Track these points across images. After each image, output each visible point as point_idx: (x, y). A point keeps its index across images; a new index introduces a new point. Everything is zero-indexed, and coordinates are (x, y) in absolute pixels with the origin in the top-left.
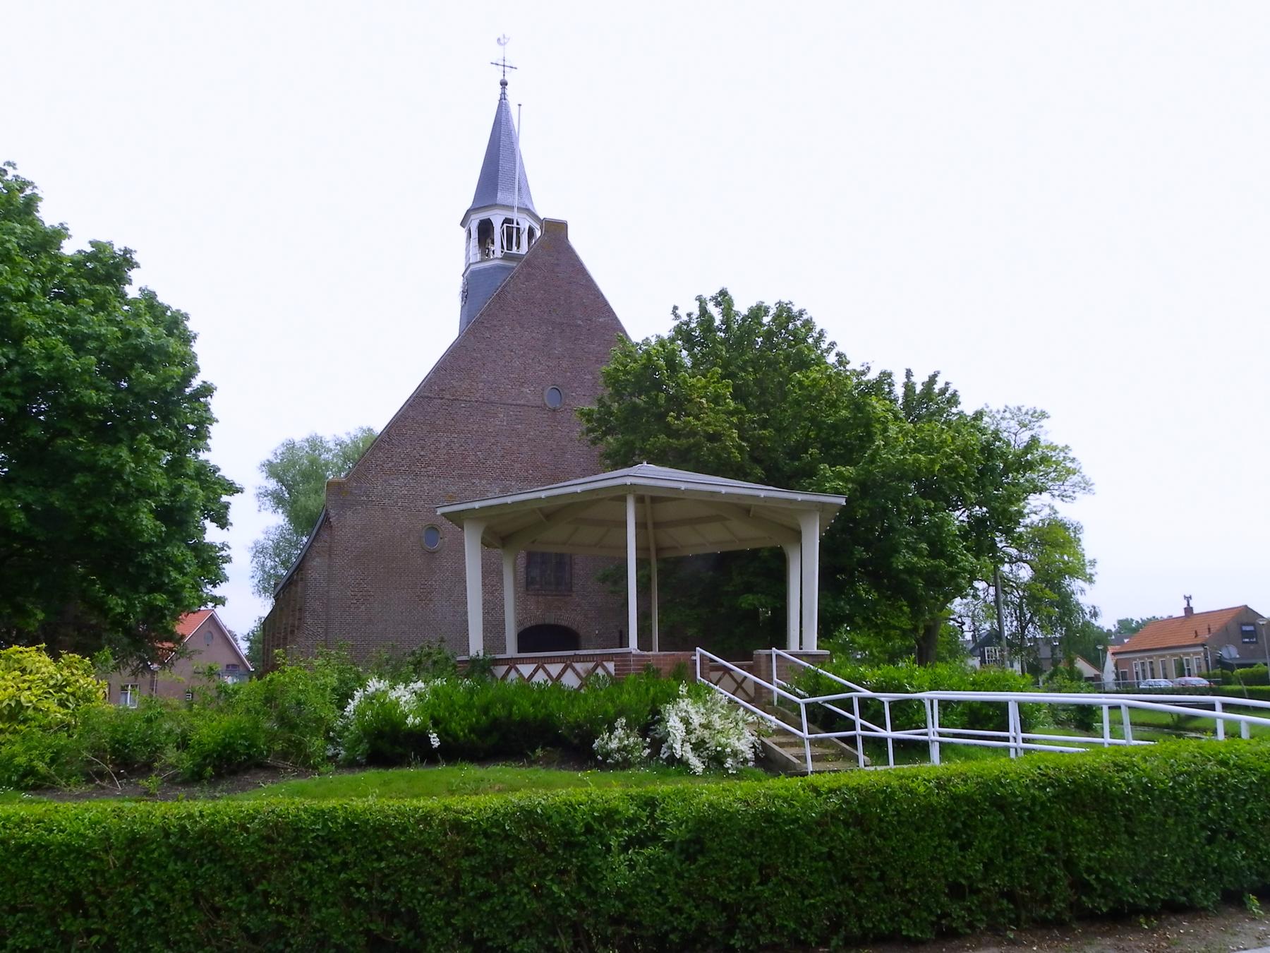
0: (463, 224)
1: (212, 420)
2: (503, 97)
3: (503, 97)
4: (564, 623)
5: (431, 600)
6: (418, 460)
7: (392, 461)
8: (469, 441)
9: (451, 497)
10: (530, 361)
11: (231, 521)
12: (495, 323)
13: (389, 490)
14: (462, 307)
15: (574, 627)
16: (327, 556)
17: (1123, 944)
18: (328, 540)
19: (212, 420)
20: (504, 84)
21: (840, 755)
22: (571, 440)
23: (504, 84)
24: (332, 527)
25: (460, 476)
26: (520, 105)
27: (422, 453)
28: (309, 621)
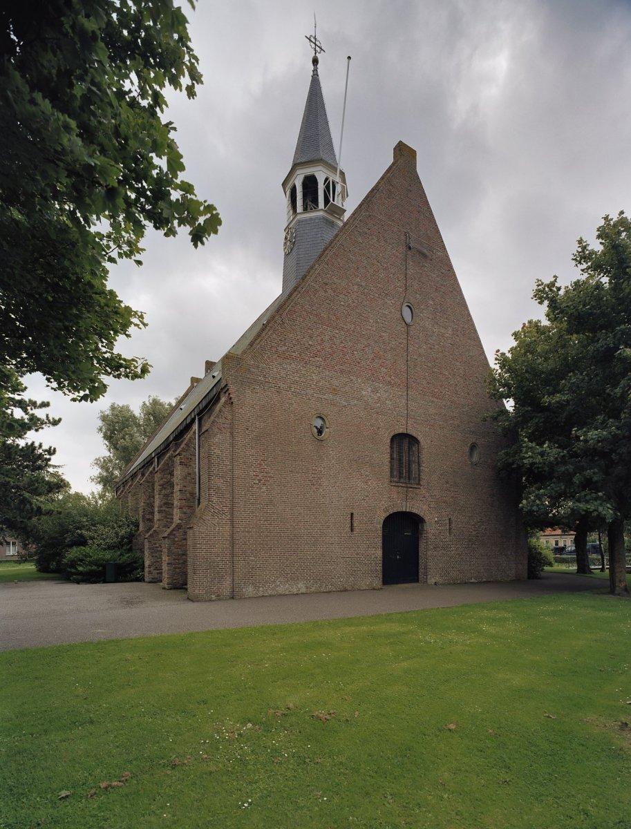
0: (284, 185)
1: (216, 232)
2: (315, 70)
3: (315, 70)
4: (415, 511)
5: (320, 485)
6: (307, 349)
7: (285, 345)
8: (348, 339)
9: (334, 389)
10: (391, 275)
11: (129, 357)
12: (366, 230)
13: (283, 373)
14: (287, 255)
15: (422, 514)
16: (228, 434)
17: (107, 203)
18: (230, 417)
19: (216, 232)
20: (315, 61)
21: (77, 175)
22: (420, 355)
23: (315, 61)
24: (232, 403)
25: (342, 371)
26: (349, 58)
27: (310, 343)
28: (215, 499)
